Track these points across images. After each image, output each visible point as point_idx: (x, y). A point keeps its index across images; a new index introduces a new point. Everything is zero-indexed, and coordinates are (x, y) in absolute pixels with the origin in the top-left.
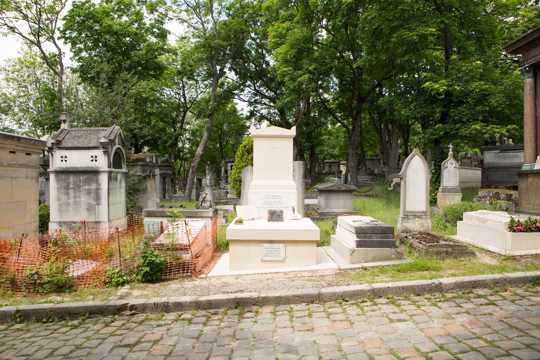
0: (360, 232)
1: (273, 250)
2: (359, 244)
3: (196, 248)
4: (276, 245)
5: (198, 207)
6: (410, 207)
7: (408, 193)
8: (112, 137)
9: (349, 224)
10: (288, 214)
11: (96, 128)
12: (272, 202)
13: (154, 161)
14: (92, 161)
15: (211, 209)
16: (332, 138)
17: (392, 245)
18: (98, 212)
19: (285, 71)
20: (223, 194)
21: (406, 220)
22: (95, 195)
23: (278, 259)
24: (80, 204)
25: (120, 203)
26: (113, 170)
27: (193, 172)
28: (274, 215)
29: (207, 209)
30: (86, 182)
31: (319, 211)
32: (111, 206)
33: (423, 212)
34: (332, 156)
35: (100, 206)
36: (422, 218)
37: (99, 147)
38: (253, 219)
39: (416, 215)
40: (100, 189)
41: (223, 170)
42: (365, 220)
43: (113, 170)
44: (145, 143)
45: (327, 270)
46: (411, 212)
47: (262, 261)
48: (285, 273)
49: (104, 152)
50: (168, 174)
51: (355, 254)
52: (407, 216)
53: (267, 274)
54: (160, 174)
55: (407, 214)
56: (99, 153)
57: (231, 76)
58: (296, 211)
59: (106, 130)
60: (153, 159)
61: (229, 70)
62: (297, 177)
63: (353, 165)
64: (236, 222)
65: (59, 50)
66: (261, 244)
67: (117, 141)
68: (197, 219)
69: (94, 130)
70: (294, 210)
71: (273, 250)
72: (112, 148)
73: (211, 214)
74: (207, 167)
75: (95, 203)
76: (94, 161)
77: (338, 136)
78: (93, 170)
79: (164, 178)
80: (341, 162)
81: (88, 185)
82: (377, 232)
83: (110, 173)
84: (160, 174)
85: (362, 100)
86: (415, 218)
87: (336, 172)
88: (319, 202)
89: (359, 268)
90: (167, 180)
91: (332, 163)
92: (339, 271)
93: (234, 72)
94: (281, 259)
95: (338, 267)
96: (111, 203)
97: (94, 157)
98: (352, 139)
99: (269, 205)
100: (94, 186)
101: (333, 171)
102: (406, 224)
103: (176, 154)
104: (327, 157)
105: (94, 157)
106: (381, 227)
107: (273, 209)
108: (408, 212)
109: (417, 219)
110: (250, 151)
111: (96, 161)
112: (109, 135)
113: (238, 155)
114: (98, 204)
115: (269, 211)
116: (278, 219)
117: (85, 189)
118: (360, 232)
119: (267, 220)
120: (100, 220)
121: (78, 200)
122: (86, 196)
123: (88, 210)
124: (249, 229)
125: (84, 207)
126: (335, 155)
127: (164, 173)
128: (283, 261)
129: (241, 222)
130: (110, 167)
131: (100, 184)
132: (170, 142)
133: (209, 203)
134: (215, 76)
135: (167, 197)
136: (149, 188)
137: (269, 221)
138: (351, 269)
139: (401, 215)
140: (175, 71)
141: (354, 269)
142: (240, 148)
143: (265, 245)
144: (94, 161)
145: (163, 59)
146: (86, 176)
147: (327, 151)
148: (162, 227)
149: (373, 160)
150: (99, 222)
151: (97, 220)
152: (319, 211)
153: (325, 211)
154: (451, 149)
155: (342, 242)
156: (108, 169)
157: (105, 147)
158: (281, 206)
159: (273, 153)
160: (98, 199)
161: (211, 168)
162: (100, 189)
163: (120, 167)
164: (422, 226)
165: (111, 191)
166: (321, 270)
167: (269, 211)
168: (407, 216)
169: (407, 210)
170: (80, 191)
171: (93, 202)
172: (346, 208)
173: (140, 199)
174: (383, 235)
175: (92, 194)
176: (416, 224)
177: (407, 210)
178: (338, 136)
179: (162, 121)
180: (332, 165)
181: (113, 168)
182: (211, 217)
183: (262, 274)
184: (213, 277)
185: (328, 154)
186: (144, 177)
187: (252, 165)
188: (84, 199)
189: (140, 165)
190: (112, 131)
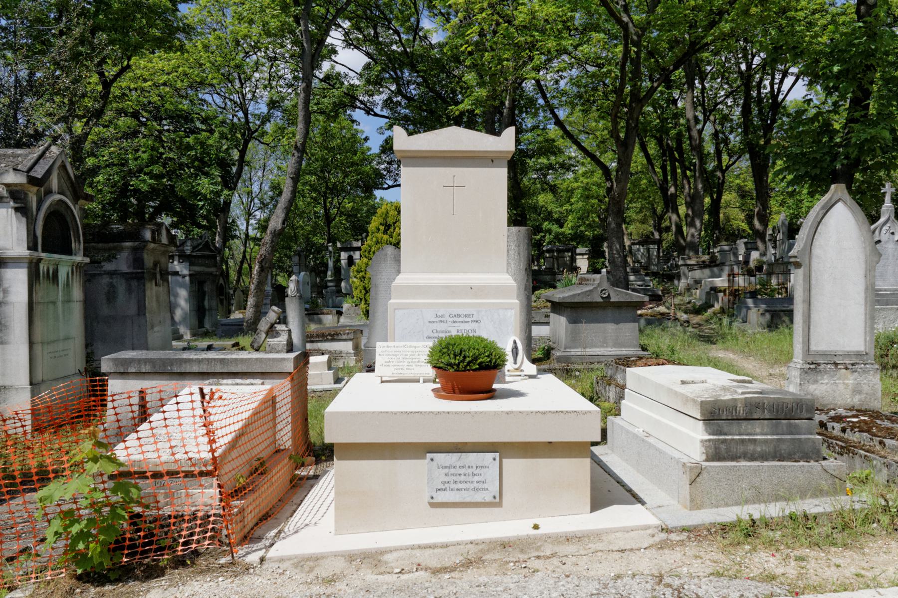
0: (715, 415)
1: (462, 471)
4: (472, 458)
5: (256, 345)
23: (479, 497)
25: (67, 338)
32: (38, 348)
33: (858, 354)
42: (712, 381)
45: (627, 530)
46: (824, 354)
47: (433, 505)
50: (211, 274)
52: (815, 366)
54: (190, 275)
68: (248, 381)
71: (462, 471)
72: (40, 202)
79: (201, 284)
80: (578, 251)
84: (190, 275)
90: (207, 288)
94: (488, 498)
96: (38, 337)
110: (391, 226)
118: (715, 415)
124: (395, 441)
127: (199, 273)
128: (497, 502)
143: (440, 458)
148: (143, 406)
154: (888, 198)
155: (651, 440)
163: (68, 251)
164: (857, 391)
168: (815, 366)
176: (841, 387)
177: (813, 348)
181: (44, 251)
187: (397, 245)
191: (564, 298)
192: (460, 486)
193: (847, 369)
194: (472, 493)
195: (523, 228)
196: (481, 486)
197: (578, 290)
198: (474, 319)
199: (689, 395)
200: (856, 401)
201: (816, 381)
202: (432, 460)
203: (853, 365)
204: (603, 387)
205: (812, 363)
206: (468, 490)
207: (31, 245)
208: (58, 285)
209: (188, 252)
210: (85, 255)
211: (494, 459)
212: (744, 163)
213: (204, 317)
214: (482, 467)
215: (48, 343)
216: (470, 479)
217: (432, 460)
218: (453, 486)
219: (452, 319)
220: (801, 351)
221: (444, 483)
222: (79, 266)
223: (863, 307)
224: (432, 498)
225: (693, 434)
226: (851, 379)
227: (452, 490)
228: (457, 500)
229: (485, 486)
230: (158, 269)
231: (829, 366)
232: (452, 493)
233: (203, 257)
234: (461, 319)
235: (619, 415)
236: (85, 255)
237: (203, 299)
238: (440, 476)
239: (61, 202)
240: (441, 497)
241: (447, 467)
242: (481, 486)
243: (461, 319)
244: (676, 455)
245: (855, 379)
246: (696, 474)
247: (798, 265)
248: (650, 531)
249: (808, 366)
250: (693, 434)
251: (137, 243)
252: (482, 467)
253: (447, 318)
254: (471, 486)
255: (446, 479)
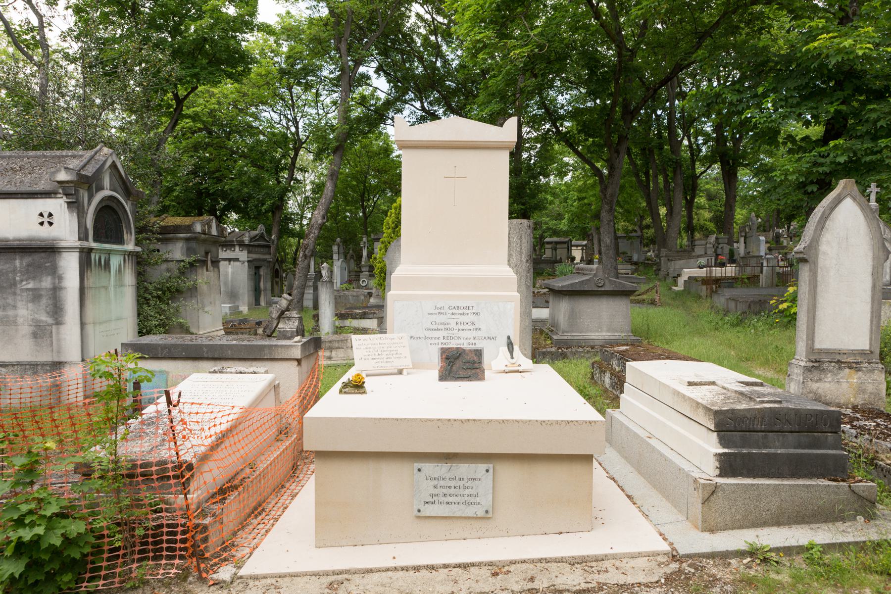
0: (729, 425)
2: (729, 466)
3: (216, 472)
4: (464, 469)
6: (826, 340)
7: (821, 302)
8: (89, 171)
9: (677, 393)
10: (496, 359)
11: (58, 153)
12: (453, 325)
13: (214, 232)
14: (42, 224)
15: (297, 338)
16: (557, 201)
17: (836, 470)
18: (59, 340)
19: (479, 41)
20: (363, 298)
21: (816, 375)
22: (50, 302)
23: (470, 511)
24: (15, 322)
25: (118, 319)
26: (94, 245)
27: (305, 256)
28: (458, 363)
29: (290, 338)
30: (27, 271)
31: (555, 337)
32: (90, 328)
33: (862, 353)
34: (555, 233)
35: (62, 327)
36: (860, 370)
37: (56, 193)
38: (400, 372)
39: (841, 361)
40: (61, 288)
41: (365, 253)
43: (94, 245)
44: (232, 206)
46: (828, 352)
47: (421, 517)
48: (497, 569)
49: (69, 203)
50: (265, 260)
51: (718, 500)
52: (821, 362)
53: (432, 568)
55: (816, 357)
56: (57, 206)
57: (381, 86)
58: (516, 348)
59: (81, 156)
60: (210, 227)
61: (375, 72)
62: (515, 259)
63: (609, 241)
64: (345, 385)
65: (40, 17)
66: (417, 465)
67: (107, 182)
69: (53, 157)
70: (510, 346)
73: (297, 353)
74: (335, 248)
75: (50, 320)
76: (46, 224)
77: (566, 199)
78: (43, 244)
79: (257, 268)
81: (34, 278)
82: (787, 427)
83: (85, 255)
85: (632, 113)
86: (840, 368)
87: (564, 257)
88: (552, 315)
89: (740, 554)
91: (557, 243)
92: (674, 566)
93: (384, 78)
94: (481, 513)
95: (665, 547)
97: (46, 215)
98: (609, 191)
99: (444, 333)
100: (47, 282)
101: (558, 258)
102: (815, 386)
103: (240, 214)
104: (546, 234)
105: (46, 215)
106: (797, 412)
107: (453, 344)
108: (821, 351)
109: (847, 370)
111: (51, 224)
112: (84, 166)
113: (388, 224)
114: (59, 323)
115: (443, 351)
116: (469, 373)
117: (28, 289)
119: (436, 374)
120: (62, 359)
121: (11, 313)
122: (30, 305)
123: (35, 335)
125: (25, 329)
126: (561, 231)
129: (357, 386)
130: (86, 239)
131: (60, 278)
132: (269, 203)
133: (296, 324)
134: (349, 80)
135: (263, 303)
136: (204, 288)
137: (442, 378)
138: (712, 556)
139: (801, 359)
140: (274, 69)
141: (723, 557)
142: (393, 211)
143: (429, 468)
144: (46, 224)
145: (250, 40)
146: (27, 260)
147: (546, 223)
149: (630, 238)
150: (60, 363)
151: (56, 359)
152: (555, 337)
153: (567, 336)
155: (653, 442)
156: (78, 244)
157: (75, 191)
158: (475, 334)
159: (454, 184)
160: (57, 311)
161: (342, 250)
162: (61, 288)
163: (121, 241)
164: (861, 390)
165: (89, 294)
166: (615, 557)
167: (443, 351)
169: (817, 346)
170: (15, 294)
171: (44, 318)
172: (615, 330)
173: (181, 309)
174: (804, 438)
175: (44, 301)
176: (845, 385)
178: (566, 199)
179: (254, 164)
180: (558, 246)
181: (96, 240)
182: (299, 361)
183: (417, 569)
184: (256, 578)
185: (548, 229)
186: (192, 265)
188: (25, 312)
189: (181, 239)
190: (92, 157)
191: (562, 286)
192: (450, 499)
193: (850, 368)
194: (462, 507)
195: (525, 221)
196: (472, 499)
197: (577, 280)
198: (474, 311)
199: (700, 401)
200: (859, 401)
201: (820, 380)
202: (419, 470)
203: (857, 363)
204: (604, 383)
205: (816, 361)
206: (458, 503)
207: (82, 236)
208: (110, 272)
209: (247, 243)
210: (136, 245)
211: (487, 471)
212: (715, 170)
213: (260, 296)
214: (474, 479)
215: (100, 323)
216: (461, 492)
217: (419, 470)
218: (442, 499)
219: (451, 311)
220: (804, 349)
221: (432, 496)
222: (131, 254)
223: (869, 306)
224: (419, 511)
225: (706, 446)
226: (855, 378)
227: (441, 503)
228: (447, 515)
229: (478, 500)
230: (209, 257)
231: (833, 364)
232: (442, 507)
233: (259, 246)
234: (460, 311)
235: (618, 407)
236: (136, 245)
237: (260, 281)
238: (427, 488)
239: (111, 198)
240: (429, 510)
241: (436, 479)
242: (472, 499)
243: (460, 311)
244: (686, 466)
245: (860, 378)
246: (711, 493)
247: (804, 261)
248: (659, 559)
249: (811, 364)
250: (706, 446)
251: (189, 235)
252: (474, 479)
253: (446, 309)
254: (463, 499)
255: (435, 491)
